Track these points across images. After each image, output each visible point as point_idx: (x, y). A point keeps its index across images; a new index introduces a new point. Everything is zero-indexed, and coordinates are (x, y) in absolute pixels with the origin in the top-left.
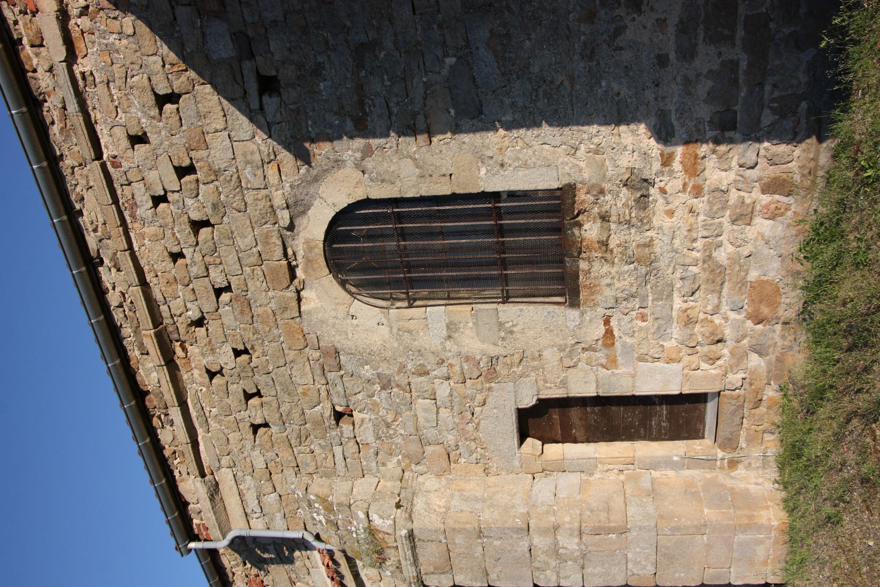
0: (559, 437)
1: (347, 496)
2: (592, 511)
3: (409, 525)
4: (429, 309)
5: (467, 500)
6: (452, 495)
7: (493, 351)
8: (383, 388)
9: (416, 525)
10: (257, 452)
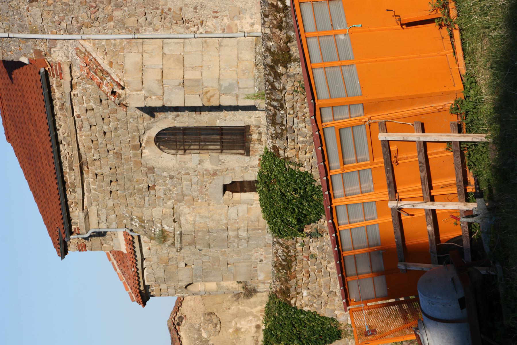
0: (239, 190)
1: (150, 216)
2: (252, 222)
3: (180, 229)
5: (202, 218)
6: (196, 216)
7: (216, 168)
8: (171, 179)
9: (183, 229)
10: (111, 200)
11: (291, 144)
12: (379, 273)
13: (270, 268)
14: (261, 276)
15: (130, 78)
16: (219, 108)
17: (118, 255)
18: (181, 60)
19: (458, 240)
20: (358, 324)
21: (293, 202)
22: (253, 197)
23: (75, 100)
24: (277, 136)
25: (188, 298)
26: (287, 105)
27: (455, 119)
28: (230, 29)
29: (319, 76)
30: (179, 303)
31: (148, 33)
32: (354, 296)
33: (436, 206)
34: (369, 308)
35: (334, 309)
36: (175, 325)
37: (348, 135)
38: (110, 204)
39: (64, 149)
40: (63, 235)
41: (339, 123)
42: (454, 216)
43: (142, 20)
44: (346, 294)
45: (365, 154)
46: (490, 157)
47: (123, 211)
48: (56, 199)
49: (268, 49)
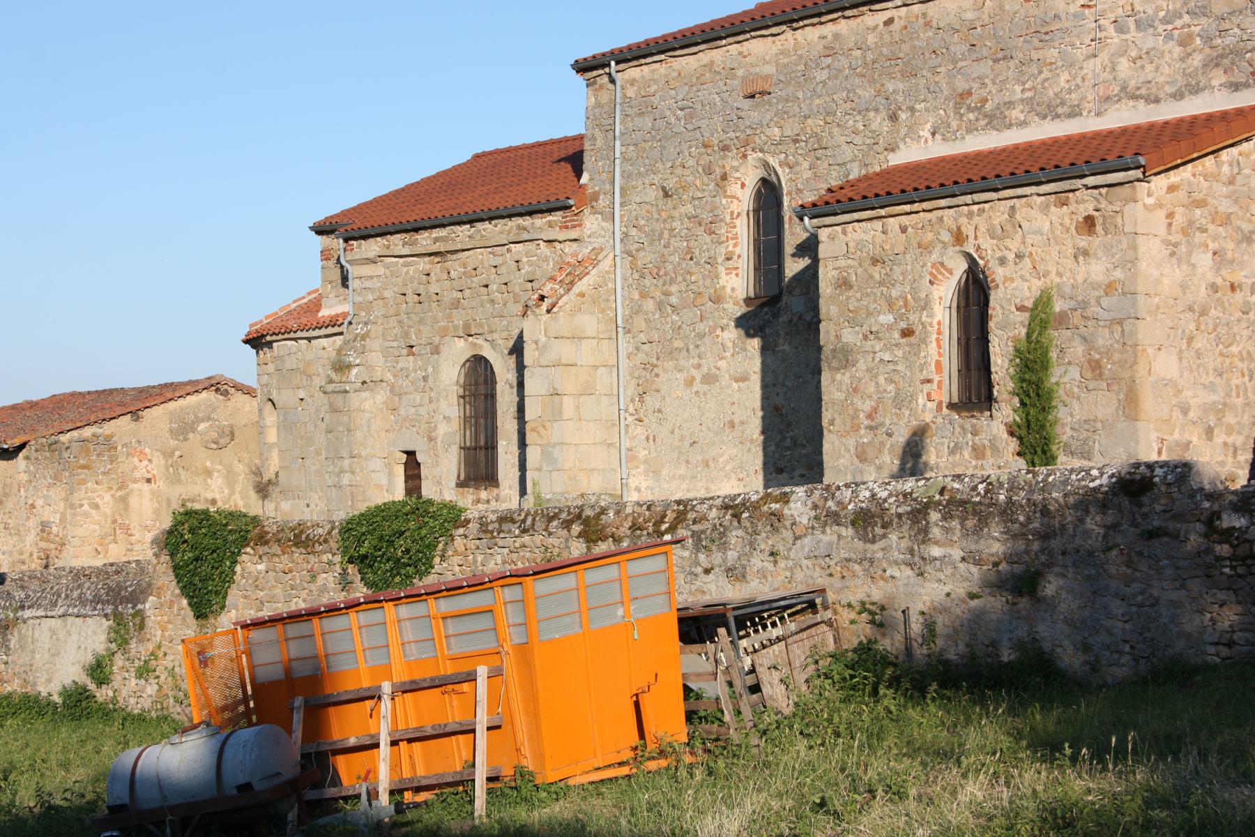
4: (850, 227)
7: (439, 440)
9: (352, 395)
11: (472, 544)
12: (288, 671)
13: (297, 518)
14: (285, 506)
15: (562, 321)
16: (522, 444)
17: (315, 305)
18: (588, 391)
19: (336, 781)
20: (218, 641)
21: (390, 549)
23: (531, 246)
24: (483, 525)
25: (255, 402)
26: (526, 539)
27: (507, 771)
28: (632, 458)
29: (565, 581)
31: (625, 346)
32: (255, 634)
34: (238, 657)
35: (240, 606)
36: (216, 385)
37: (485, 622)
38: (387, 294)
41: (500, 609)
42: (370, 774)
44: (258, 624)
45: (457, 648)
46: (454, 823)
47: (378, 311)
49: (603, 511)
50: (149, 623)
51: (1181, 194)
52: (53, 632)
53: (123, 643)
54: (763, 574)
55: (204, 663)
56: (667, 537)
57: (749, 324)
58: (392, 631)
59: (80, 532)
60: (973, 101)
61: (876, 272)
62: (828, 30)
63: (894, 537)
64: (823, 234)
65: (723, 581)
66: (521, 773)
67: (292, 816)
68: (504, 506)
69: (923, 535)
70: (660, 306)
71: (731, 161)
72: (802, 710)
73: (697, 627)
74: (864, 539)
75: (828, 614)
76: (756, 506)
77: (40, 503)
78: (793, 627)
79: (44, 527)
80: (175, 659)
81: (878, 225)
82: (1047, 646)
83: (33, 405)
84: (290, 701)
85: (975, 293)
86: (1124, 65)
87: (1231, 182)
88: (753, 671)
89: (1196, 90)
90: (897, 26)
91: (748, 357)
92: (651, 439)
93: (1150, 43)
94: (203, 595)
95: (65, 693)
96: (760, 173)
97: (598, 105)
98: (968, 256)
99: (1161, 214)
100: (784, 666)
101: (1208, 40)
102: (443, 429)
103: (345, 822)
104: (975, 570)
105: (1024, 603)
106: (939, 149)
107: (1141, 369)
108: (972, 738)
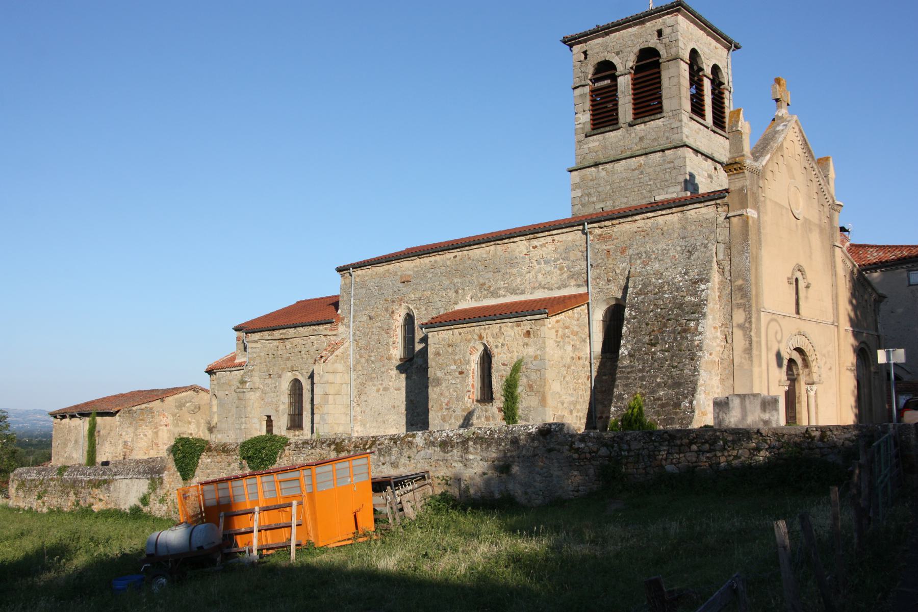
11: (292, 453)
12: (218, 502)
13: (223, 441)
14: (219, 436)
15: (329, 366)
16: (313, 414)
17: (234, 358)
18: (338, 393)
19: (236, 546)
20: (191, 490)
21: (260, 454)
22: (264, 432)
23: (318, 337)
24: (297, 445)
25: (209, 396)
26: (313, 451)
27: (304, 542)
28: (355, 419)
29: (328, 468)
30: (206, 391)
31: (353, 375)
32: (206, 487)
33: (256, 533)
34: (199, 497)
35: (200, 476)
36: (194, 389)
37: (296, 484)
38: (262, 354)
39: (292, 331)
40: (246, 329)
41: (302, 479)
42: (249, 543)
43: (360, 373)
44: (207, 483)
45: (285, 493)
46: (283, 563)
47: (258, 361)
48: (264, 326)
49: (343, 440)
50: (165, 482)
51: (561, 323)
52: (127, 485)
53: (154, 489)
54: (405, 465)
55: (185, 498)
56: (368, 451)
57: (401, 368)
58: (260, 487)
59: (139, 445)
60: (486, 287)
61: (450, 349)
62: (433, 259)
63: (455, 451)
64: (430, 335)
65: (390, 468)
66: (309, 543)
67: (219, 559)
68: (305, 438)
69: (466, 450)
70: (367, 361)
71: (395, 307)
72: (419, 518)
73: (379, 486)
74: (444, 452)
75: (430, 481)
76: (403, 439)
77: (124, 434)
78: (416, 486)
79: (125, 443)
80: (174, 496)
81: (450, 332)
82: (512, 493)
83: (123, 395)
84: (219, 514)
85: (487, 359)
86: (540, 276)
87: (578, 320)
88: (400, 503)
89: (565, 286)
90: (458, 258)
91: (400, 381)
92: (363, 412)
93: (549, 269)
94: (186, 468)
95: (131, 509)
96: (407, 311)
97: (345, 284)
98: (484, 345)
99: (554, 331)
100: (412, 501)
101: (569, 269)
102: (282, 407)
103: (239, 562)
104: (486, 464)
105: (504, 476)
106: (474, 304)
107: (547, 388)
108: (483, 528)
